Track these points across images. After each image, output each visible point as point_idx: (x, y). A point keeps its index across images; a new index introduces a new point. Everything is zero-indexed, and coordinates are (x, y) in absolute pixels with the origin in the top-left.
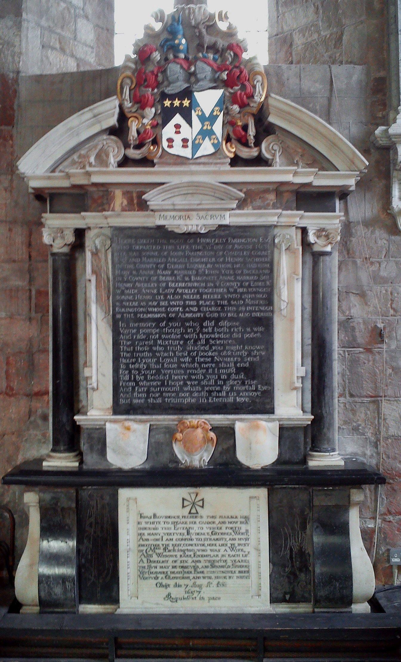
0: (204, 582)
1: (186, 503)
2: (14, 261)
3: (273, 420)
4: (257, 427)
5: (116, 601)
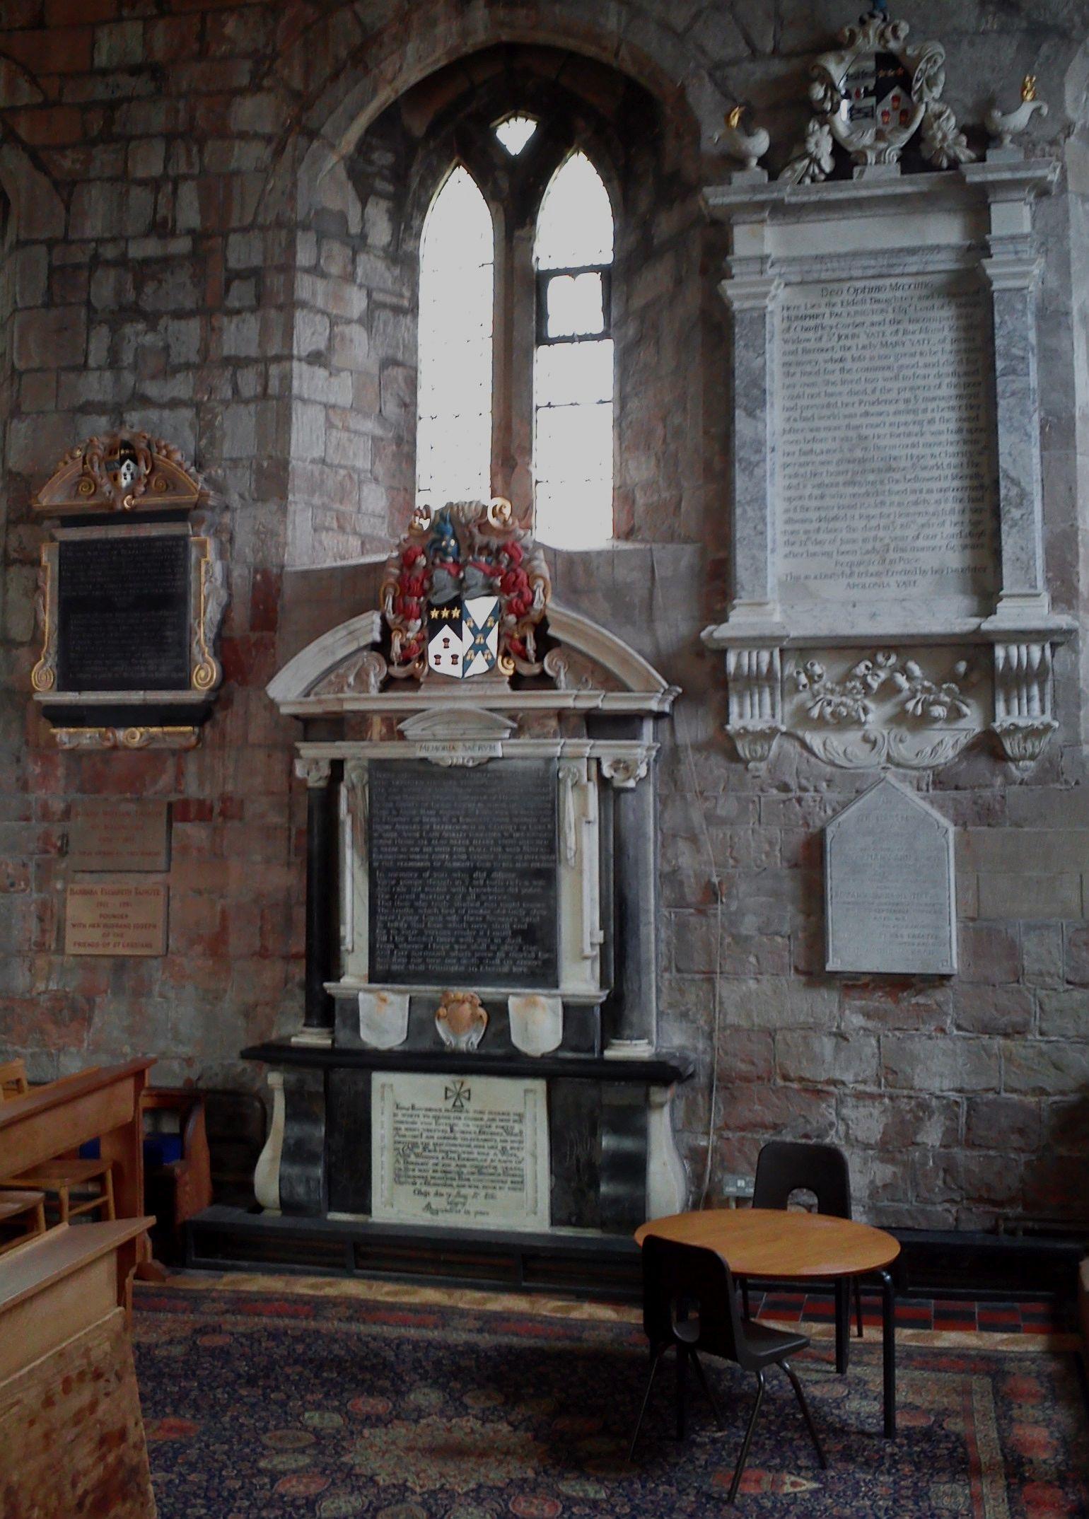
0: (470, 1192)
1: (449, 1094)
2: (273, 793)
3: (554, 996)
4: (534, 1004)
5: (367, 1210)
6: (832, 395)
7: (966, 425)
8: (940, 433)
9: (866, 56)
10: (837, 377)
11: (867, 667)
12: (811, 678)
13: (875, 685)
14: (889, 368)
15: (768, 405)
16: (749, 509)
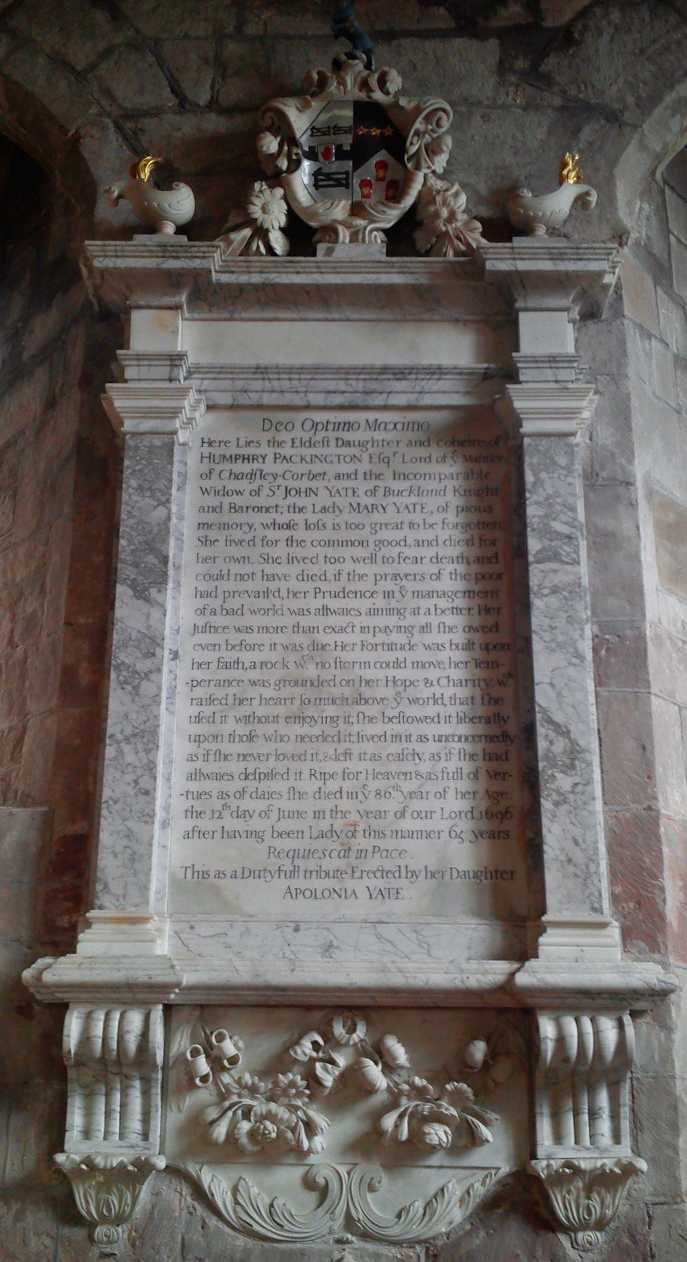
6: (273, 577)
7: (478, 638)
8: (439, 647)
9: (341, 104)
10: (281, 551)
11: (315, 1044)
12: (217, 1063)
13: (328, 1081)
14: (361, 543)
15: (170, 585)
16: (126, 748)
